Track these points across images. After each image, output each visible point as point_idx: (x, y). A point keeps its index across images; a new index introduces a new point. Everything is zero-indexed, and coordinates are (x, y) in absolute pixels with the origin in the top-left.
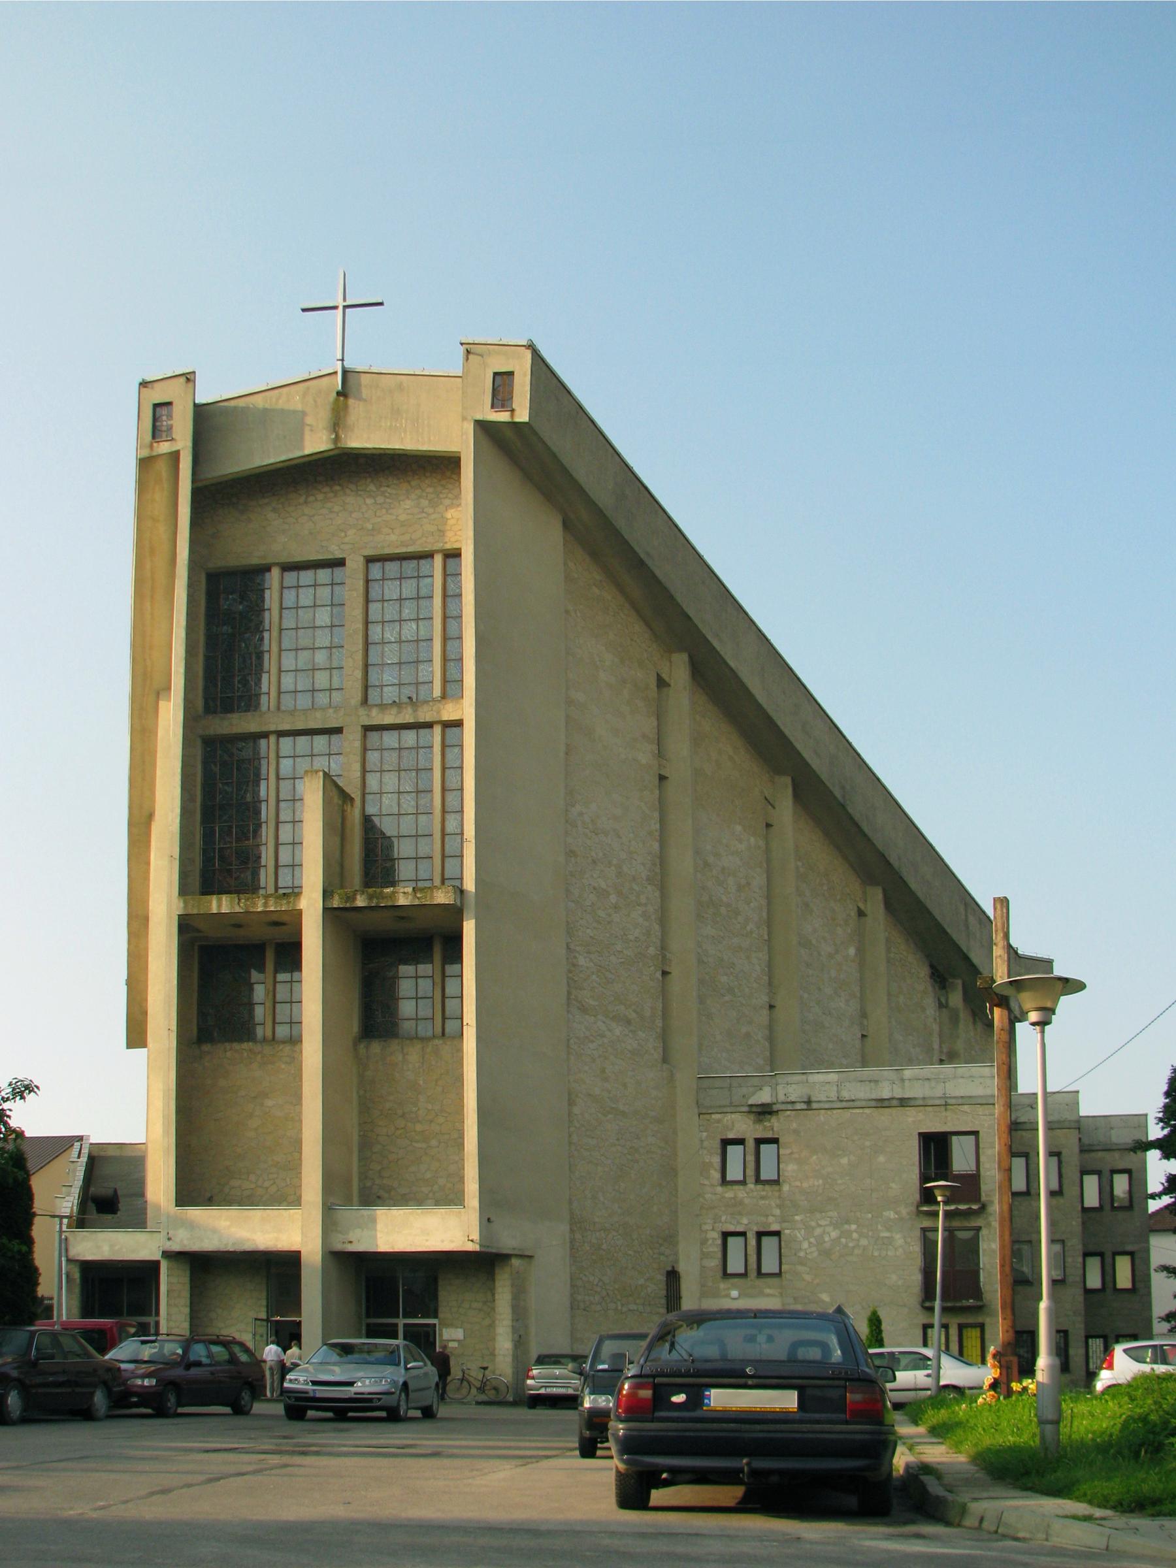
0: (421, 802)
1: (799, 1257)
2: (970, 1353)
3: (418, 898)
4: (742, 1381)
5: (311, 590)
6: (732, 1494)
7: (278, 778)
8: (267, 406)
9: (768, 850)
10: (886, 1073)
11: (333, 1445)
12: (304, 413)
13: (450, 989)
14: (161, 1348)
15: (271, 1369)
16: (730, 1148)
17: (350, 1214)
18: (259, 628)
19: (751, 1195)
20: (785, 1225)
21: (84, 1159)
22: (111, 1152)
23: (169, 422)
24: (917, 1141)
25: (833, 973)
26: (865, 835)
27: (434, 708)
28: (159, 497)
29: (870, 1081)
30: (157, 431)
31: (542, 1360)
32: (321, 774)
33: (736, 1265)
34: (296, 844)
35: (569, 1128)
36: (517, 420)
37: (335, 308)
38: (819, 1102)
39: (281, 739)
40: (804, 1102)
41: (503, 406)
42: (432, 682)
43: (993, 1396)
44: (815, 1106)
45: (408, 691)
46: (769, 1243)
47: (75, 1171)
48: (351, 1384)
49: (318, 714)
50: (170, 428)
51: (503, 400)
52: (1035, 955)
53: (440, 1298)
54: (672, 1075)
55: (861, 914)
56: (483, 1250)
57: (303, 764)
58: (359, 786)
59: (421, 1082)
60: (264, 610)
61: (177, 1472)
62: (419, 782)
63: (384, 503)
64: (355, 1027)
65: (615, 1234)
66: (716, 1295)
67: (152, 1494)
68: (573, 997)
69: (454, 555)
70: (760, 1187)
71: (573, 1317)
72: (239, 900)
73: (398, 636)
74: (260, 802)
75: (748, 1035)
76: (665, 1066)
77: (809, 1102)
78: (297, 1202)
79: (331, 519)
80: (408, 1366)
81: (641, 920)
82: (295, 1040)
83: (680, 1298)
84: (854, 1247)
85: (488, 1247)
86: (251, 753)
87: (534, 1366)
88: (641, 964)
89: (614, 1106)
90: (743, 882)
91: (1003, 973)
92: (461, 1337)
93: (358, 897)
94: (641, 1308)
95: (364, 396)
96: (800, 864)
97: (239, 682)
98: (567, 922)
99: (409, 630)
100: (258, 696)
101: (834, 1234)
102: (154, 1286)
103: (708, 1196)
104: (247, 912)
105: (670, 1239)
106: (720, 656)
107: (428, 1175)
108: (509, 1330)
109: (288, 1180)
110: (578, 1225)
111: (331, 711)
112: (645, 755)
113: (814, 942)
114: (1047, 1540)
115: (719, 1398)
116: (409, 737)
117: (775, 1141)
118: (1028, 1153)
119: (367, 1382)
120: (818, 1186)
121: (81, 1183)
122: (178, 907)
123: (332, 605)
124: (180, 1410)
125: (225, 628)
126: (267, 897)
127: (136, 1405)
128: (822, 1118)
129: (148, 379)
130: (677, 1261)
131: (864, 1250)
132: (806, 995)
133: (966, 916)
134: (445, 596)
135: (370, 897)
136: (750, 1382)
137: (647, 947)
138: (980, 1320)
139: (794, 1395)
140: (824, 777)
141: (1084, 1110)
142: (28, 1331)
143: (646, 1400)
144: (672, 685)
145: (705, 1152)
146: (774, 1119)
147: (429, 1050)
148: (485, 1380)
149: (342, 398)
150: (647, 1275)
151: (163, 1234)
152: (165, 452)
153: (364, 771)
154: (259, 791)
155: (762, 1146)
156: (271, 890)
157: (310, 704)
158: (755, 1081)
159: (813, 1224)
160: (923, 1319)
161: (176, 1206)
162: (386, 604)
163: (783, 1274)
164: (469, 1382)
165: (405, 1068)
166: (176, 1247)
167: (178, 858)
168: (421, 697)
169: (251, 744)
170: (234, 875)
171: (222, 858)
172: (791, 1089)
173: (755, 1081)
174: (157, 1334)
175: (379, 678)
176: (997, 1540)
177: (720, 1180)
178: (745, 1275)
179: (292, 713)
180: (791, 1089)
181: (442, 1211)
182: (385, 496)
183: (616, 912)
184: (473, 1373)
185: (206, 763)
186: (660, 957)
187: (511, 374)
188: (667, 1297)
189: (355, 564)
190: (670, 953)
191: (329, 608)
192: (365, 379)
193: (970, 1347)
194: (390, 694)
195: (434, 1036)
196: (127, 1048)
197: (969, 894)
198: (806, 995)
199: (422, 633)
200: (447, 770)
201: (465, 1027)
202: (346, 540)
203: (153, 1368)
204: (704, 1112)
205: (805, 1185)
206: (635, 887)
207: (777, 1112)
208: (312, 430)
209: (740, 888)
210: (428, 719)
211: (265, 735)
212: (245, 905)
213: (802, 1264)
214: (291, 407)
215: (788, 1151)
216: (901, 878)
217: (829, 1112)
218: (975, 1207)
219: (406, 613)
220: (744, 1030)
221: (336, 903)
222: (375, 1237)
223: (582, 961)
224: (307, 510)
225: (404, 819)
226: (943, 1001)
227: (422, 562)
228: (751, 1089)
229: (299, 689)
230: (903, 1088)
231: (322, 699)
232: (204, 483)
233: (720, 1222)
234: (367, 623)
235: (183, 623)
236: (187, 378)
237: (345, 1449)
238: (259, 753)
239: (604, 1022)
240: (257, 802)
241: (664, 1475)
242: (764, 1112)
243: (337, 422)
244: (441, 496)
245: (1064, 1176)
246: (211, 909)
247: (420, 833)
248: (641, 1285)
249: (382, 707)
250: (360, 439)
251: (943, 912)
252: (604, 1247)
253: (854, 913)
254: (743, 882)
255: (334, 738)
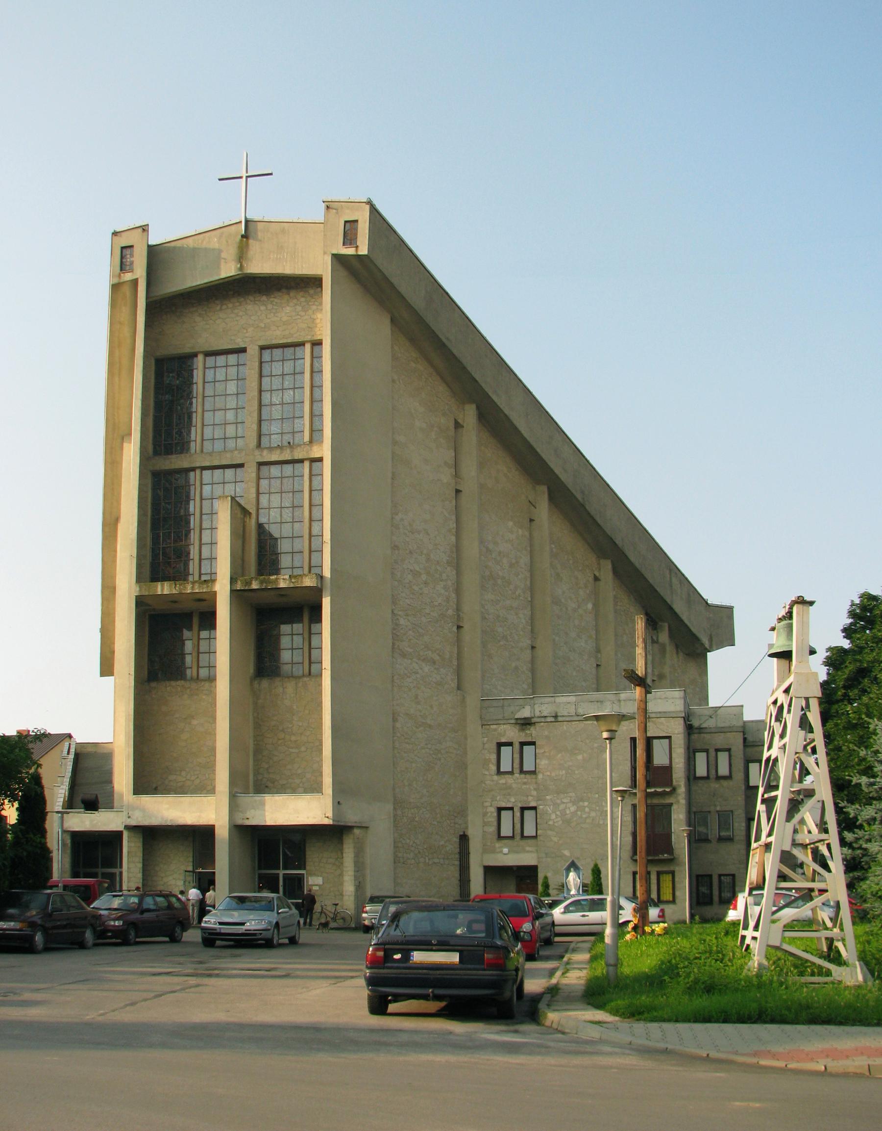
0: (296, 514)
1: (549, 825)
2: (665, 892)
3: (293, 582)
4: (430, 947)
5: (224, 369)
6: (433, 1006)
7: (202, 499)
8: (196, 246)
9: (531, 538)
10: (608, 696)
11: (227, 969)
12: (220, 251)
13: (314, 643)
14: (125, 900)
15: (193, 905)
16: (502, 748)
17: (246, 800)
18: (189, 396)
19: (516, 781)
20: (540, 802)
21: (72, 756)
22: (90, 749)
23: (131, 259)
24: (629, 743)
25: (577, 622)
26: (599, 525)
27: (305, 449)
28: (125, 311)
29: (597, 701)
30: (124, 265)
31: (373, 900)
32: (230, 498)
33: (506, 831)
34: (213, 544)
35: (393, 737)
36: (360, 253)
37: (241, 177)
38: (563, 716)
39: (204, 472)
40: (553, 717)
41: (351, 244)
42: (303, 431)
43: (634, 935)
44: (560, 719)
45: (287, 438)
46: (529, 814)
47: (66, 765)
48: (243, 924)
49: (228, 455)
50: (132, 263)
51: (351, 240)
52: (720, 604)
53: (307, 856)
54: (464, 698)
55: (596, 579)
56: (335, 823)
57: (218, 490)
58: (255, 504)
59: (295, 707)
60: (193, 384)
61: (138, 991)
62: (295, 500)
63: (273, 308)
64: (251, 670)
65: (425, 810)
66: (493, 851)
67: (126, 1005)
68: (396, 646)
69: (318, 343)
70: (523, 776)
71: (395, 868)
72: (176, 585)
73: (281, 400)
74: (190, 515)
75: (516, 668)
76: (459, 691)
77: (556, 717)
78: (212, 791)
79: (237, 320)
80: (280, 911)
81: (443, 591)
82: (212, 679)
83: (469, 853)
84: (586, 818)
85: (339, 821)
86: (184, 482)
87: (368, 904)
88: (443, 621)
89: (424, 721)
90: (514, 561)
91: (642, 664)
92: (321, 883)
93: (253, 582)
94: (442, 861)
95: (260, 237)
96: (553, 546)
97: (176, 433)
98: (393, 595)
99: (288, 396)
100: (189, 442)
101: (573, 809)
102: (119, 851)
103: (488, 782)
104: (181, 594)
105: (461, 812)
106: (496, 404)
107: (299, 771)
108: (353, 878)
109: (207, 775)
110: (399, 805)
111: (236, 452)
112: (446, 476)
113: (563, 600)
114: (576, 1034)
115: (418, 957)
116: (288, 469)
117: (533, 743)
118: (708, 749)
119: (253, 922)
120: (562, 775)
121: (70, 774)
122: (135, 591)
123: (238, 379)
124: (138, 940)
125: (167, 396)
126: (193, 583)
127: (110, 937)
128: (565, 728)
129: (118, 230)
130: (467, 828)
131: (593, 820)
132: (557, 639)
133: (671, 578)
134: (312, 372)
135: (261, 582)
136: (434, 948)
137: (447, 610)
138: (672, 868)
139: (458, 954)
140: (570, 486)
141: (746, 718)
142: (46, 894)
143: (380, 957)
144: (465, 425)
145: (486, 751)
146: (532, 728)
147: (300, 684)
148: (336, 913)
149: (245, 239)
150: (447, 838)
151: (125, 814)
152: (128, 279)
153: (258, 493)
154: (189, 508)
155: (524, 747)
156: (196, 578)
157: (223, 447)
158: (521, 702)
159: (559, 801)
160: (632, 868)
161: (134, 795)
162: (273, 378)
163: (538, 837)
164: (325, 914)
165: (284, 697)
166: (133, 822)
167: (135, 556)
168: (296, 442)
169: (184, 476)
170: (173, 566)
171: (164, 554)
172: (543, 707)
173: (521, 702)
174: (121, 890)
175: (268, 429)
176: (551, 1034)
177: (496, 771)
178: (512, 837)
179: (211, 454)
180: (543, 707)
181: (308, 797)
182: (273, 305)
183: (425, 587)
184: (329, 908)
185: (154, 489)
186: (456, 617)
187: (356, 221)
188: (460, 853)
189: (253, 351)
190: (463, 613)
191: (236, 382)
192: (260, 226)
193: (664, 887)
194: (276, 440)
195: (303, 675)
196: (101, 676)
197: (673, 563)
198: (557, 639)
199: (297, 397)
200: (313, 492)
201: (323, 671)
202: (247, 335)
203: (120, 914)
204: (486, 723)
205: (553, 774)
206: (439, 568)
207: (535, 723)
208: (226, 262)
209: (511, 565)
210: (301, 457)
211: (193, 469)
212: (179, 588)
213: (551, 830)
214: (211, 246)
215: (542, 751)
216: (623, 553)
217: (569, 723)
218: (668, 790)
219: (287, 384)
220: (514, 665)
221: (239, 586)
222: (265, 816)
223: (402, 621)
224: (222, 315)
225: (285, 526)
226: (655, 638)
227: (297, 349)
228: (517, 708)
229: (216, 437)
230: (620, 706)
231: (231, 444)
232: (154, 299)
233: (496, 800)
234: (260, 391)
235: (140, 396)
236: (143, 229)
237: (234, 972)
238: (189, 482)
239: (417, 663)
240: (188, 515)
241: (390, 998)
242: (526, 723)
243: (242, 255)
244: (310, 303)
245: (733, 765)
246: (157, 592)
247: (295, 535)
248: (442, 845)
249: (271, 449)
250: (259, 266)
251: (654, 578)
252: (417, 819)
253: (591, 579)
254: (514, 561)
255: (239, 470)
